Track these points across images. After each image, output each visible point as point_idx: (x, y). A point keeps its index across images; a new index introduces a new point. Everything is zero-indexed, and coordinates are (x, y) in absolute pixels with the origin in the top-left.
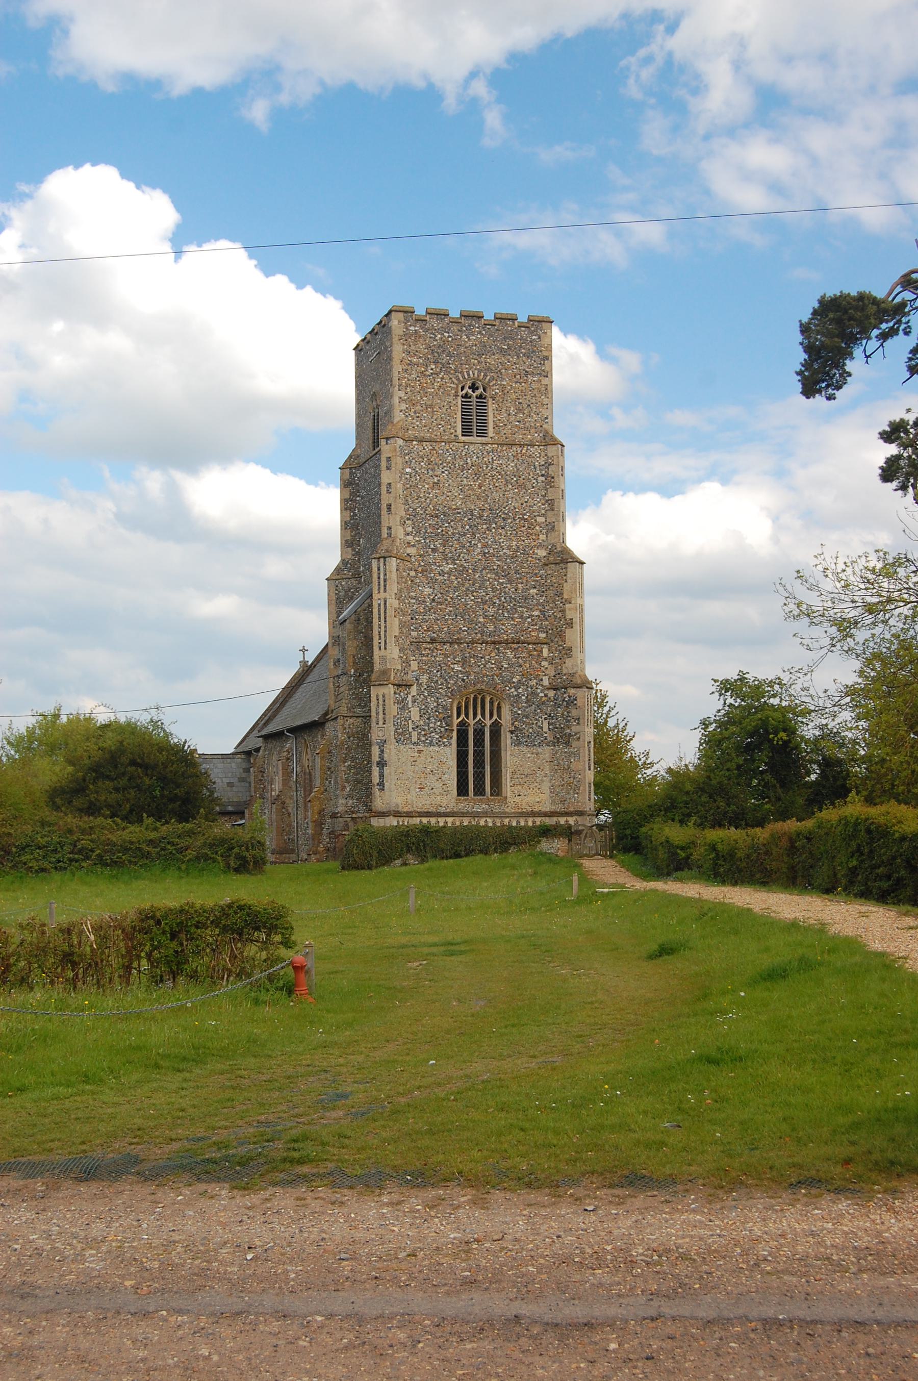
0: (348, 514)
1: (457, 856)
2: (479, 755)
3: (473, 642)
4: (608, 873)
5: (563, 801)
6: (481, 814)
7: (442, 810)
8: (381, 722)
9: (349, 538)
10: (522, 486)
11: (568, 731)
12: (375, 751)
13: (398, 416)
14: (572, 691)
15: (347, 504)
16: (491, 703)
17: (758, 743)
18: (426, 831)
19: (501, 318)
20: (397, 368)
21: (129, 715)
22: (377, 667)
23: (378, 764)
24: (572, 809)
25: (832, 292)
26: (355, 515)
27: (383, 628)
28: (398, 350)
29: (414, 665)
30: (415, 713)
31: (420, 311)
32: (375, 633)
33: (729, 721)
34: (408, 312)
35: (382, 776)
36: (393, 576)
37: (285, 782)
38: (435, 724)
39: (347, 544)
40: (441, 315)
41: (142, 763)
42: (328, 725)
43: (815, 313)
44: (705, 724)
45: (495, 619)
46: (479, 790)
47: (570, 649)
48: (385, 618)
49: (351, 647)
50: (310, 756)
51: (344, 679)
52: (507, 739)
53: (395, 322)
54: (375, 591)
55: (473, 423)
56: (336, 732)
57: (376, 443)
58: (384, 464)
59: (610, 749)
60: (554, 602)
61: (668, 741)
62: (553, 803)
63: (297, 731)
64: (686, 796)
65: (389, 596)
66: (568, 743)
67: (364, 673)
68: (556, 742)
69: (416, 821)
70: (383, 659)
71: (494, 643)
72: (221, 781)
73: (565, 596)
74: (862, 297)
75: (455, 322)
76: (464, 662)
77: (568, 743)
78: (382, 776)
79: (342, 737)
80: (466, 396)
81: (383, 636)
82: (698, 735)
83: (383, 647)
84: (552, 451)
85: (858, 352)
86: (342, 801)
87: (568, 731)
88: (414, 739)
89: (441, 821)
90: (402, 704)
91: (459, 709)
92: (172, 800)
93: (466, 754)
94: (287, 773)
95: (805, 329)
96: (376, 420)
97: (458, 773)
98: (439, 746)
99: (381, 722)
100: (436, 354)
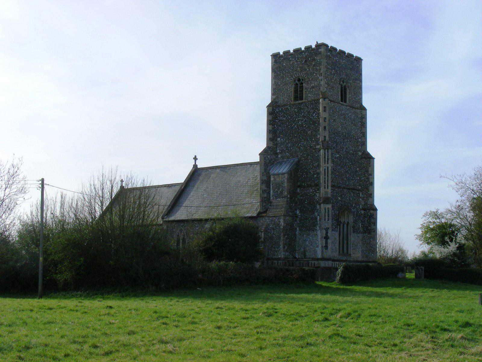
0: (271, 127)
5: (367, 257)
8: (327, 220)
9: (272, 137)
11: (370, 228)
24: (371, 260)
26: (275, 127)
27: (326, 179)
48: (328, 175)
54: (321, 164)
60: (364, 174)
62: (363, 257)
66: (369, 233)
68: (364, 232)
73: (369, 173)
77: (369, 233)
81: (326, 183)
83: (326, 187)
87: (370, 228)
98: (335, 231)
99: (327, 220)
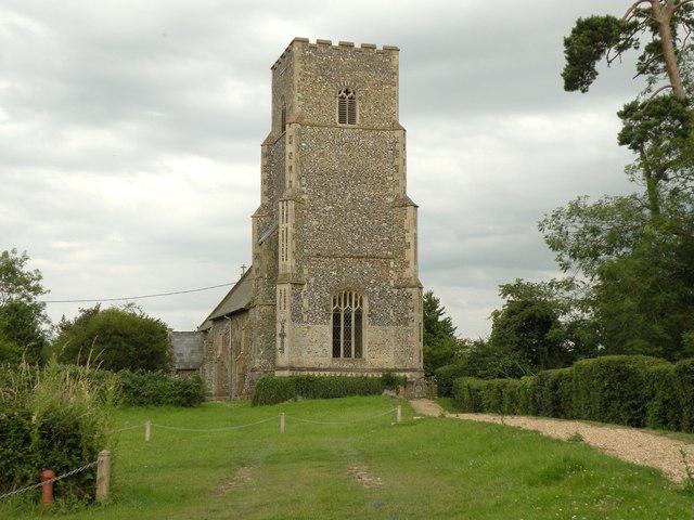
1: (327, 397)
2: (348, 331)
3: (345, 256)
4: (429, 408)
5: (402, 362)
6: (348, 369)
7: (322, 366)
10: (378, 156)
12: (279, 327)
13: (297, 110)
14: (409, 290)
15: (266, 169)
16: (356, 297)
17: (528, 324)
18: (310, 380)
19: (366, 47)
20: (297, 78)
21: (114, 303)
22: (281, 271)
23: (280, 335)
25: (585, 16)
28: (297, 66)
29: (306, 271)
30: (305, 303)
31: (313, 41)
32: (280, 250)
33: (510, 313)
34: (305, 42)
35: (282, 343)
36: (291, 213)
37: (224, 349)
38: (319, 310)
39: (265, 194)
40: (327, 44)
41: (102, 330)
42: (251, 310)
43: (574, 31)
44: (496, 314)
45: (359, 242)
46: (348, 354)
47: (408, 262)
49: (266, 260)
50: (236, 332)
51: (261, 280)
52: (365, 320)
53: (295, 49)
55: (347, 114)
56: (255, 315)
57: (284, 128)
58: (287, 139)
59: (435, 328)
61: (473, 319)
63: (232, 315)
64: (480, 358)
65: (286, 226)
66: (406, 324)
67: (273, 276)
69: (306, 373)
70: (285, 266)
71: (358, 257)
72: (183, 353)
74: (608, 19)
75: (335, 49)
76: (339, 269)
77: (406, 324)
78: (282, 343)
79: (259, 318)
80: (342, 97)
82: (491, 323)
84: (398, 134)
85: (604, 58)
86: (258, 360)
88: (305, 319)
89: (322, 374)
90: (297, 297)
91: (334, 300)
92: (142, 358)
93: (339, 337)
94: (225, 343)
95: (567, 43)
96: (284, 113)
97: (334, 342)
100: (322, 70)
